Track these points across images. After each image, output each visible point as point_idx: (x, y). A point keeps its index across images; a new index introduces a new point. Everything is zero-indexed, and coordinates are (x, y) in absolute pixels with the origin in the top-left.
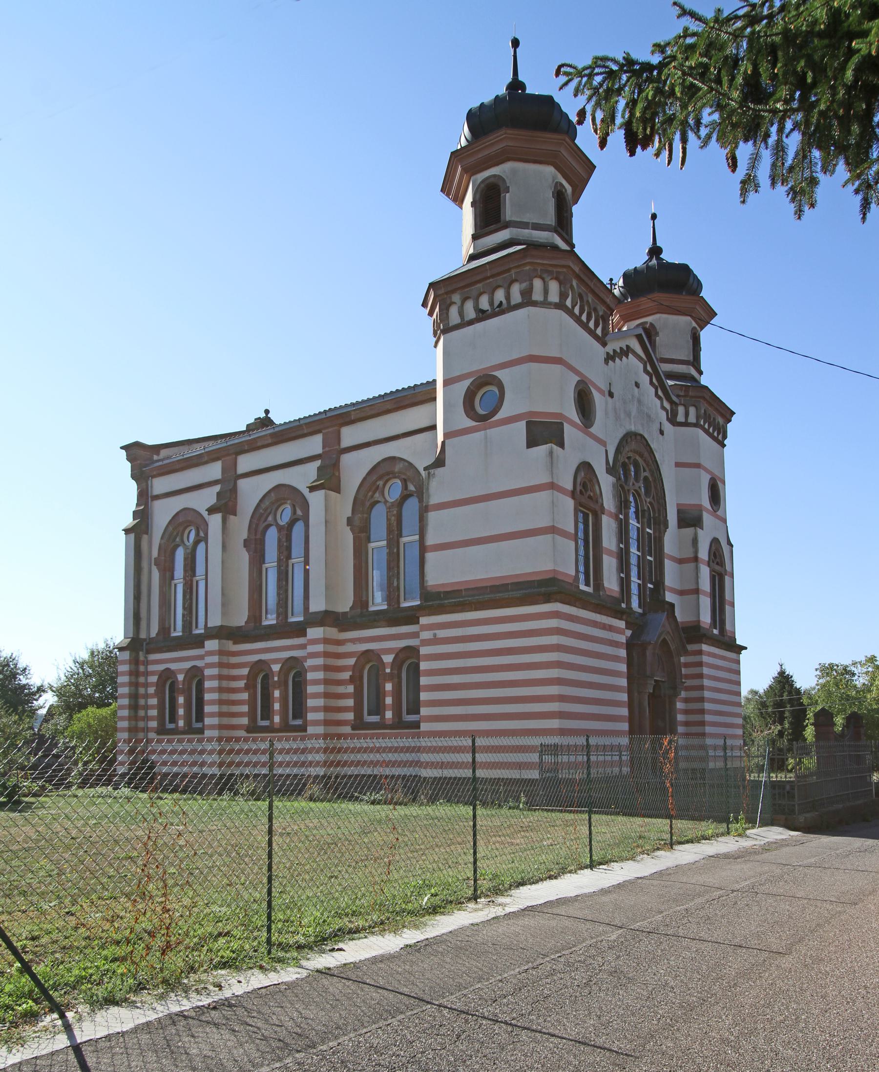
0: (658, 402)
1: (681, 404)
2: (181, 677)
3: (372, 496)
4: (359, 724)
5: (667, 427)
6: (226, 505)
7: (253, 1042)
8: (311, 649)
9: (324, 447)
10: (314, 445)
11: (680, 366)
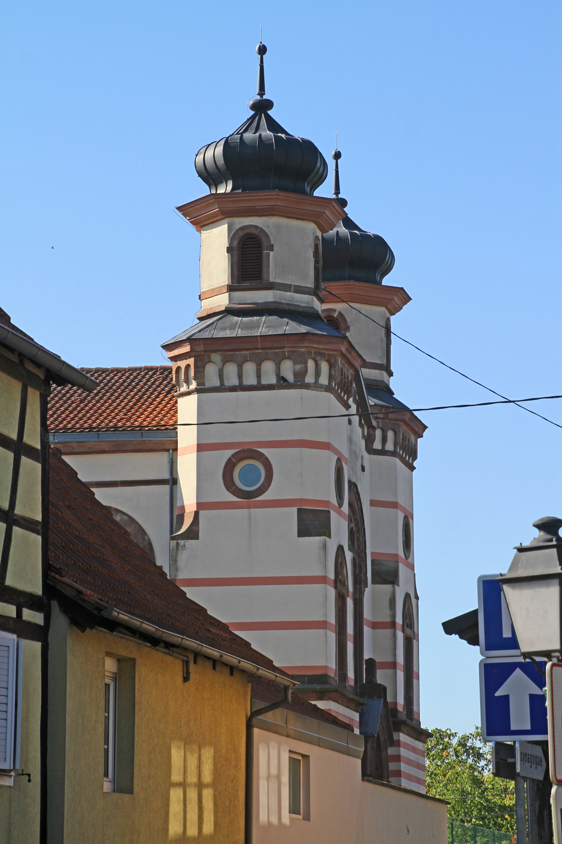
0: (360, 430)
1: (378, 427)
7: (461, 835)
11: (373, 371)
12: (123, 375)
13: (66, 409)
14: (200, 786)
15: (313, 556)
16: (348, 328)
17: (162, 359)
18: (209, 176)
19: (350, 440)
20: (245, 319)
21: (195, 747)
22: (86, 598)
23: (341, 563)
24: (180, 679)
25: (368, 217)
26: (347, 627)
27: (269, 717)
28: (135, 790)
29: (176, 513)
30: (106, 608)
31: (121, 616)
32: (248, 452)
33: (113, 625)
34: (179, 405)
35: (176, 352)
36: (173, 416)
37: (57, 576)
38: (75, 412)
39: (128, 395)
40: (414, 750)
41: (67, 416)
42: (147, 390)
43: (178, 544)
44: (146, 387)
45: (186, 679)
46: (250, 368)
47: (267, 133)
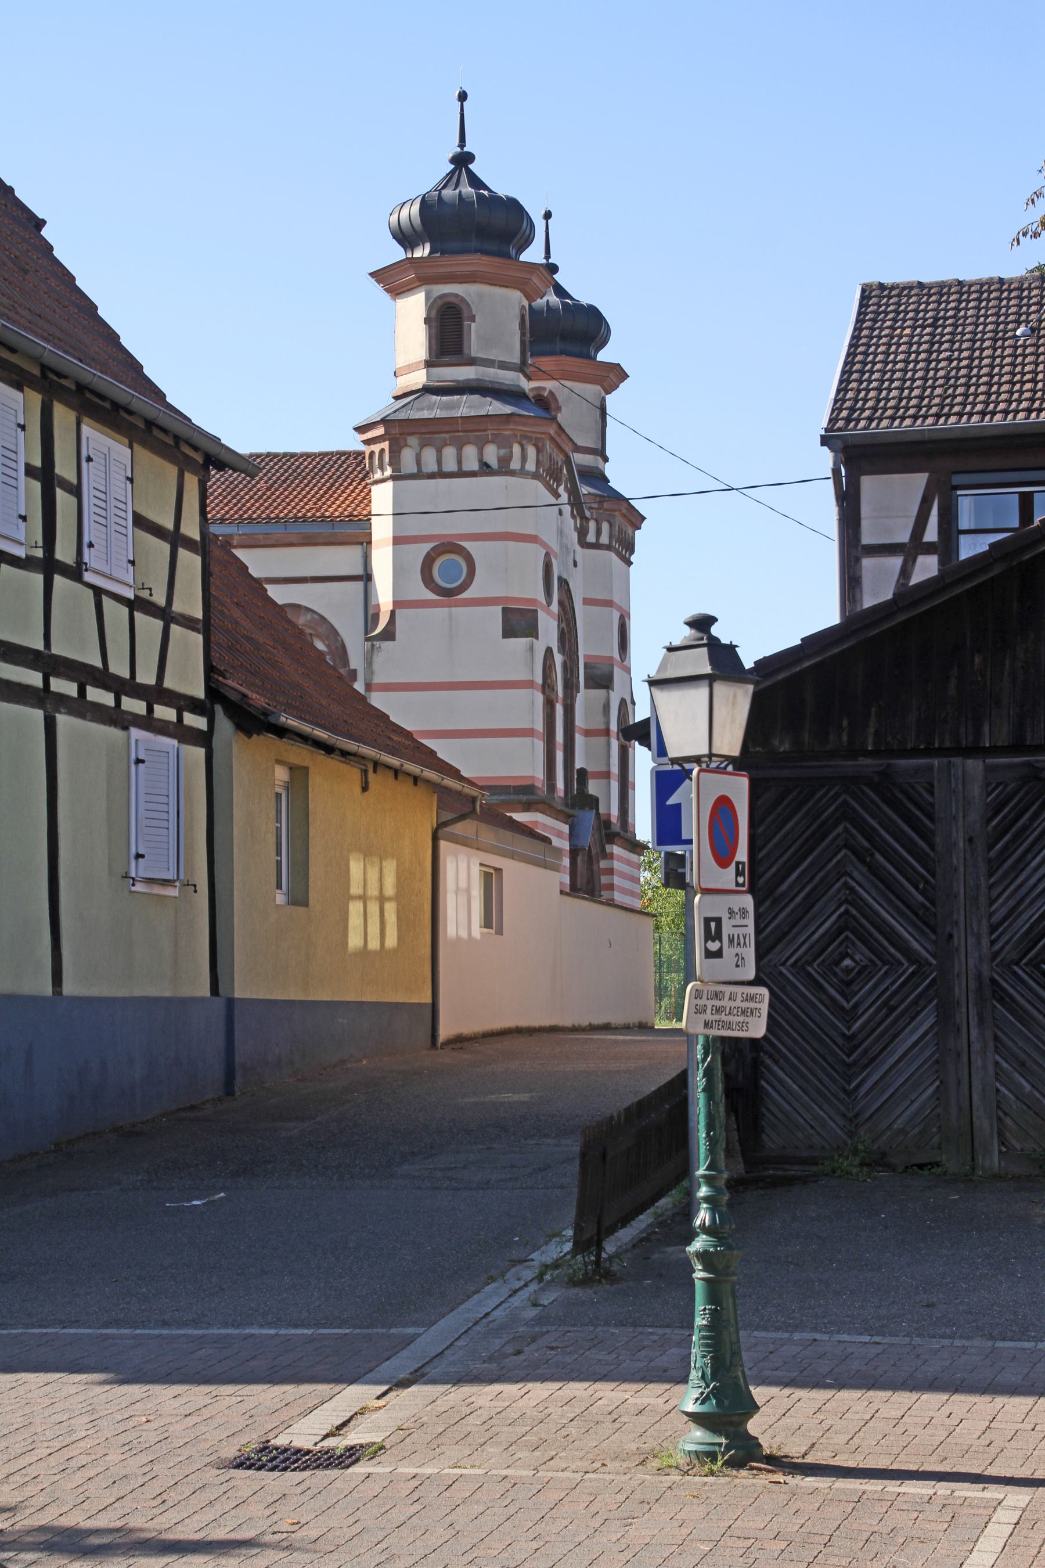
0: (572, 521)
5: (580, 553)
12: (313, 460)
13: (251, 497)
14: (382, 899)
15: (519, 660)
16: (559, 409)
17: (354, 443)
18: (404, 237)
19: (561, 533)
20: (444, 398)
21: (376, 860)
22: (251, 702)
23: (550, 667)
24: (358, 789)
25: (581, 283)
26: (558, 733)
27: (458, 828)
28: (310, 903)
29: (371, 612)
30: (273, 713)
31: (289, 721)
32: (448, 546)
33: (281, 732)
34: (373, 494)
35: (370, 435)
36: (367, 505)
37: (220, 679)
38: (261, 501)
39: (318, 482)
40: (629, 863)
41: (253, 505)
42: (339, 477)
43: (373, 646)
44: (338, 473)
45: (365, 789)
46: (449, 453)
47: (467, 190)
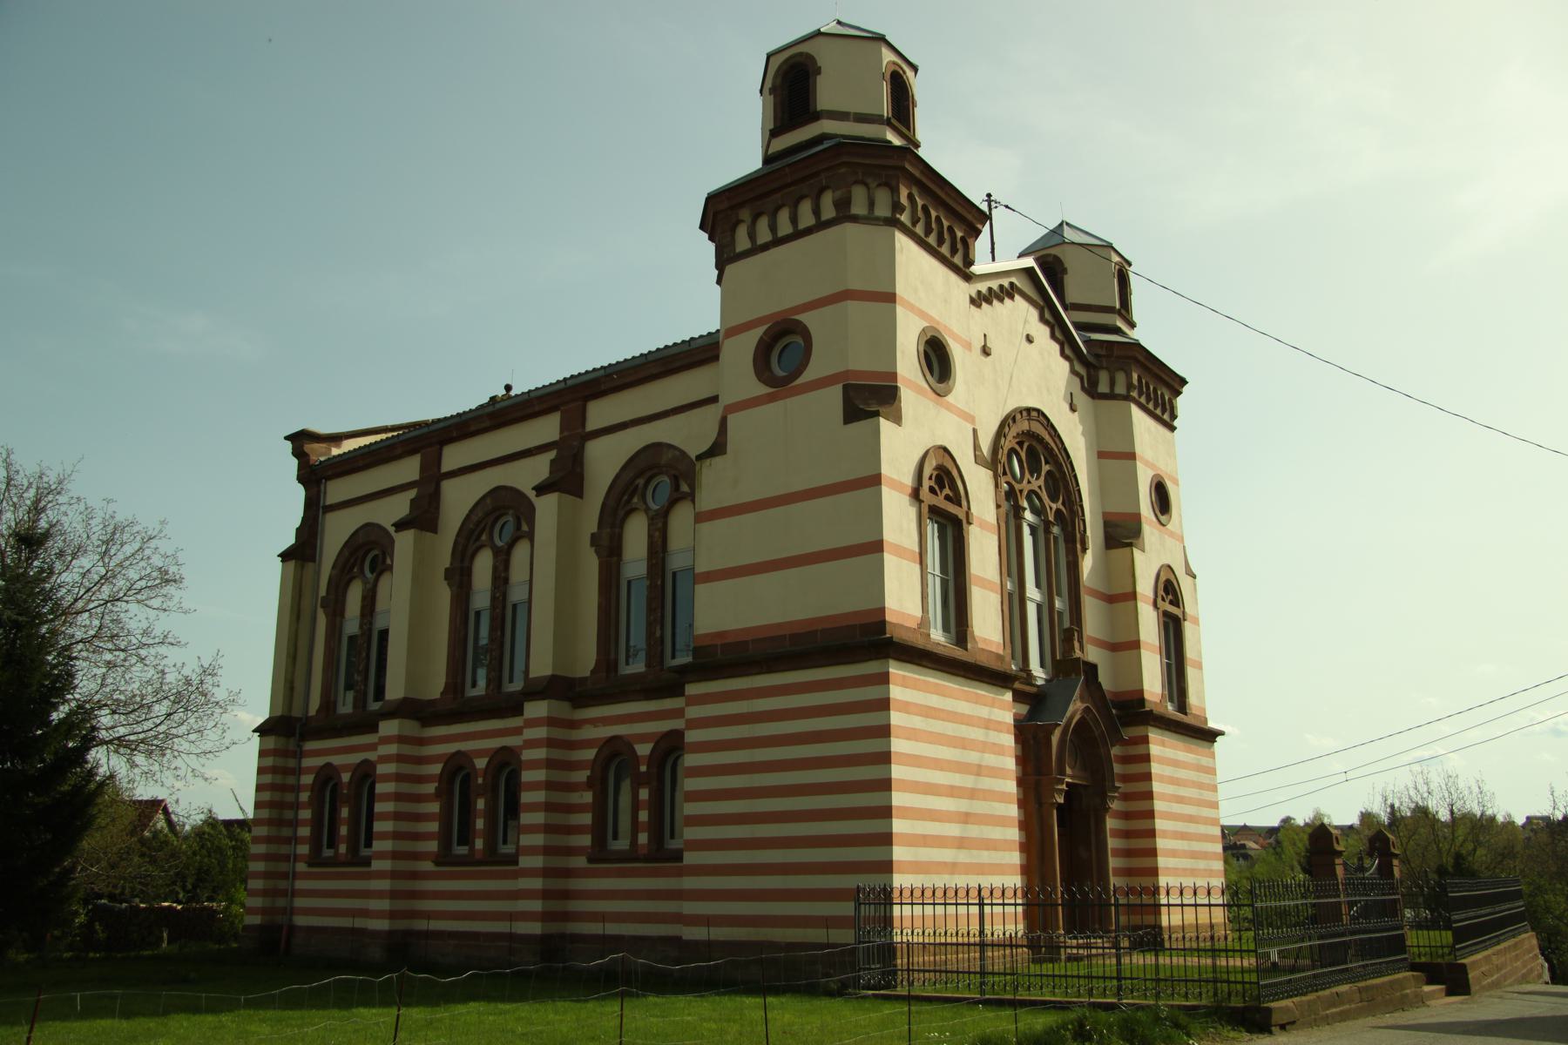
2: (346, 777)
3: (629, 501)
4: (600, 854)
6: (424, 517)
8: (530, 734)
9: (562, 432)
10: (547, 429)
